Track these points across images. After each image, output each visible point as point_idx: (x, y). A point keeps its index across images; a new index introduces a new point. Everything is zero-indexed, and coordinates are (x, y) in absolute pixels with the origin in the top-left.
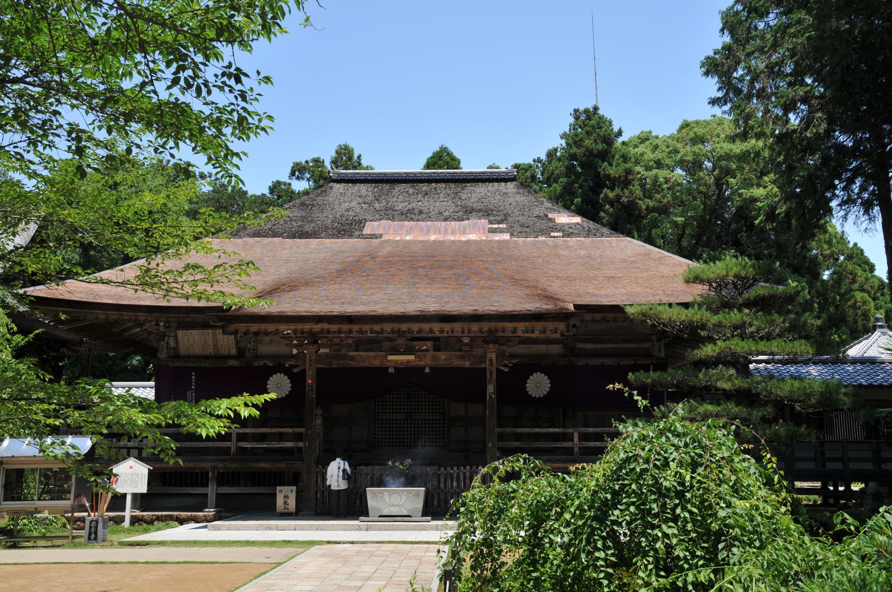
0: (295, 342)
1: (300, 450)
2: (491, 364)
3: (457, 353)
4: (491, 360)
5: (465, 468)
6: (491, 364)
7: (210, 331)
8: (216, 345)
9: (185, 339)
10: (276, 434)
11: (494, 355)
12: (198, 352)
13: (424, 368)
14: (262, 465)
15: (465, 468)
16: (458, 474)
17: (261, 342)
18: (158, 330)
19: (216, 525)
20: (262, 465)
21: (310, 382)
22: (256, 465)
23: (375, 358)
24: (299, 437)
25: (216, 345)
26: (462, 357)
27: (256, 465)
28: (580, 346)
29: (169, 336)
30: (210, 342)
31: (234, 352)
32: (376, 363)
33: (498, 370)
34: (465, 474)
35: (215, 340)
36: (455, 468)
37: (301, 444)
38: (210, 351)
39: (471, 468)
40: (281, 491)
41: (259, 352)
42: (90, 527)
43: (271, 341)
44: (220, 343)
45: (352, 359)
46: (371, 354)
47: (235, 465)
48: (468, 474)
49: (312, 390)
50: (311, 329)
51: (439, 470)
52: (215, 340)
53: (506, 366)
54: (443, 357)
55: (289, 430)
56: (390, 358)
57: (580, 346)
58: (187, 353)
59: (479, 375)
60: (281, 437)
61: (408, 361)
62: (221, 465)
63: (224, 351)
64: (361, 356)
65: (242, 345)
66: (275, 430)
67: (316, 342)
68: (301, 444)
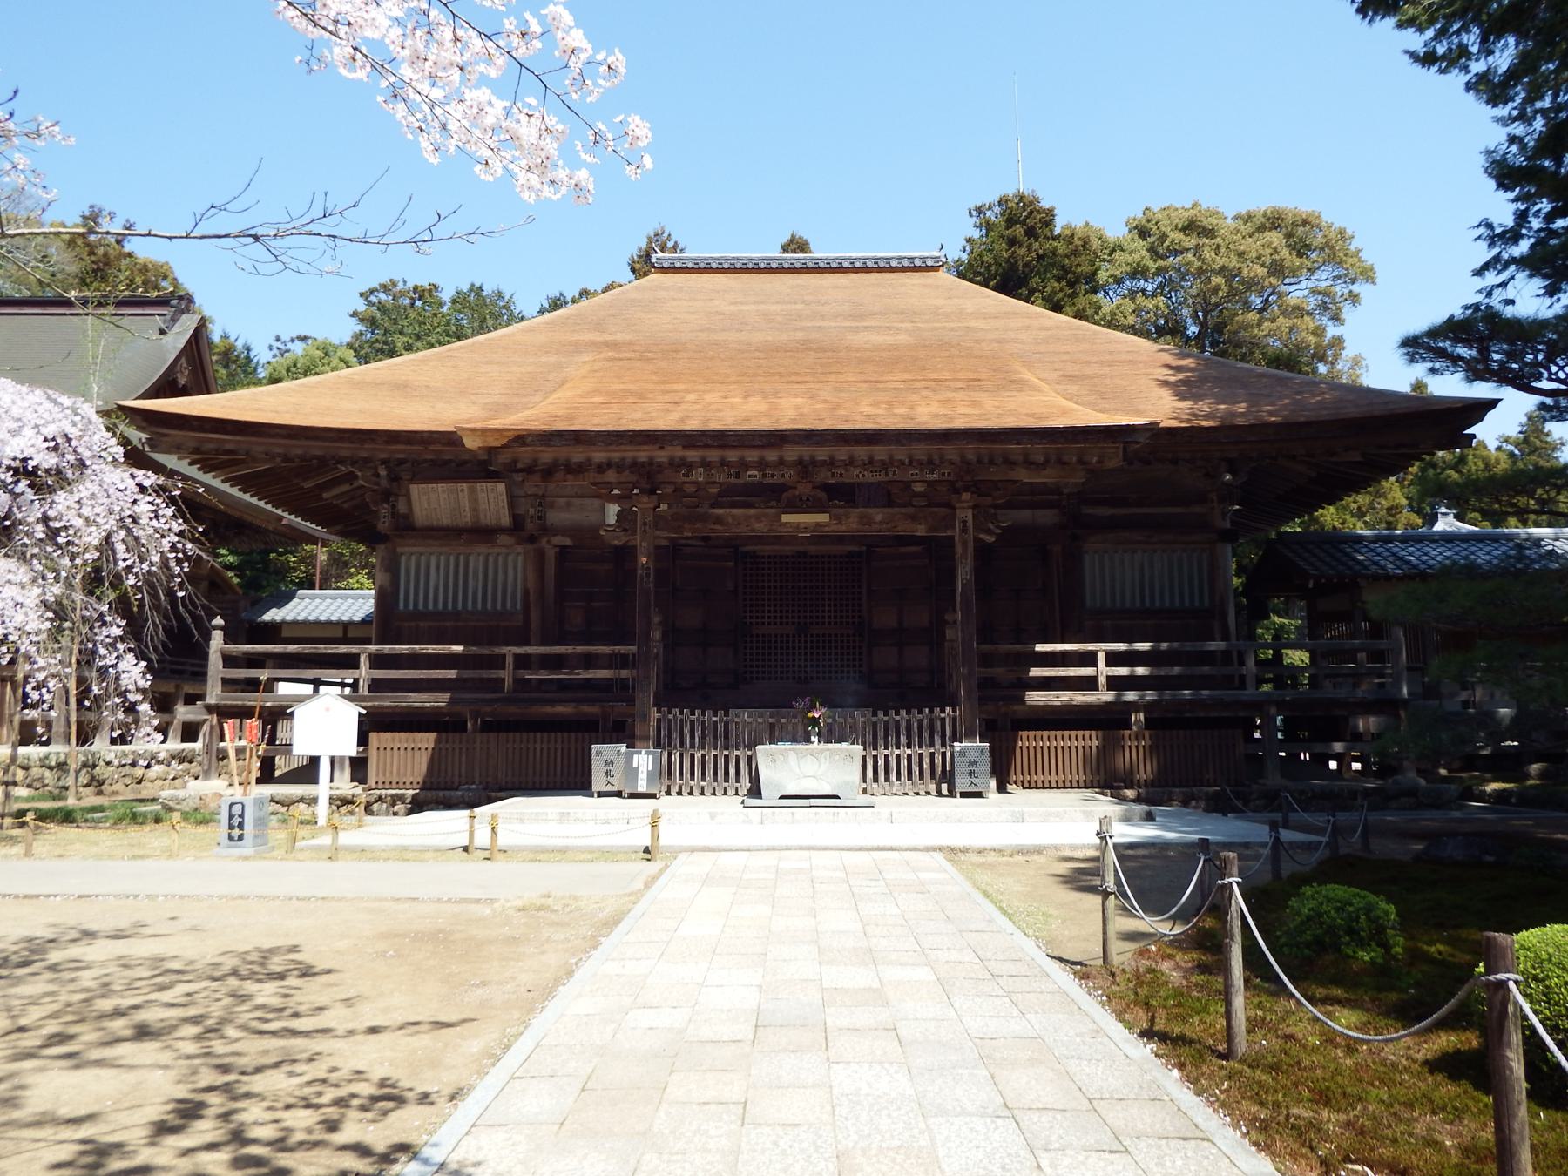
0: (616, 491)
1: (623, 684)
2: (964, 530)
3: (903, 510)
4: (964, 523)
5: (920, 712)
6: (964, 530)
7: (465, 486)
8: (475, 510)
9: (424, 498)
10: (580, 655)
11: (970, 513)
12: (446, 520)
13: (1484, 40)
14: (560, 709)
15: (920, 712)
16: (908, 721)
17: (552, 506)
18: (377, 484)
19: (1127, 413)
20: (560, 709)
21: (644, 560)
22: (548, 709)
23: (758, 518)
24: (621, 661)
25: (475, 510)
26: (913, 518)
27: (548, 709)
28: (1090, 511)
29: (397, 495)
30: (465, 503)
31: (506, 521)
32: (761, 528)
33: (976, 539)
34: (920, 721)
35: (474, 501)
36: (903, 712)
37: (624, 673)
38: (466, 519)
39: (931, 712)
40: (599, 753)
41: (549, 523)
42: (231, 817)
43: (569, 505)
44: (483, 506)
45: (719, 520)
46: (752, 511)
47: (512, 709)
48: (925, 722)
49: (648, 575)
50: (651, 459)
51: (875, 714)
52: (474, 501)
53: (989, 532)
54: (879, 518)
55: (606, 650)
56: (786, 518)
57: (1090, 511)
58: (427, 523)
59: (939, 551)
60: (589, 661)
61: (818, 525)
62: (488, 709)
63: (487, 520)
64: (733, 516)
65: (521, 511)
66: (580, 649)
67: (652, 492)
68: (624, 673)
